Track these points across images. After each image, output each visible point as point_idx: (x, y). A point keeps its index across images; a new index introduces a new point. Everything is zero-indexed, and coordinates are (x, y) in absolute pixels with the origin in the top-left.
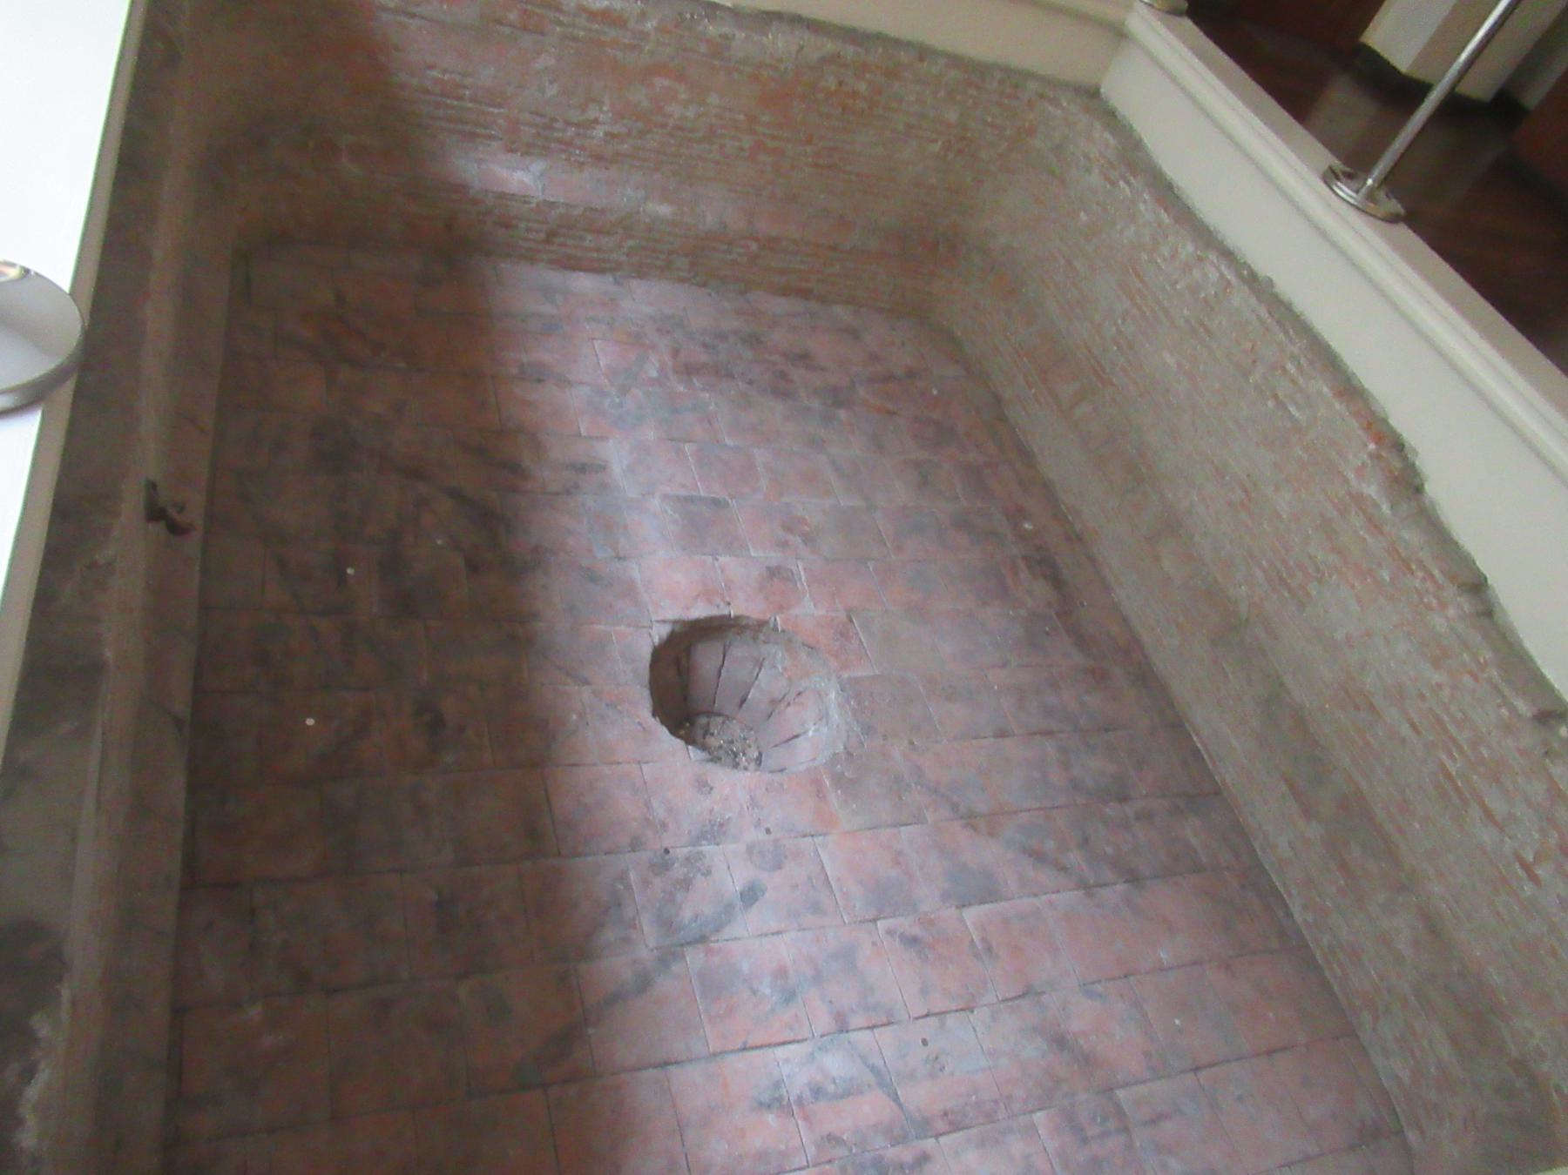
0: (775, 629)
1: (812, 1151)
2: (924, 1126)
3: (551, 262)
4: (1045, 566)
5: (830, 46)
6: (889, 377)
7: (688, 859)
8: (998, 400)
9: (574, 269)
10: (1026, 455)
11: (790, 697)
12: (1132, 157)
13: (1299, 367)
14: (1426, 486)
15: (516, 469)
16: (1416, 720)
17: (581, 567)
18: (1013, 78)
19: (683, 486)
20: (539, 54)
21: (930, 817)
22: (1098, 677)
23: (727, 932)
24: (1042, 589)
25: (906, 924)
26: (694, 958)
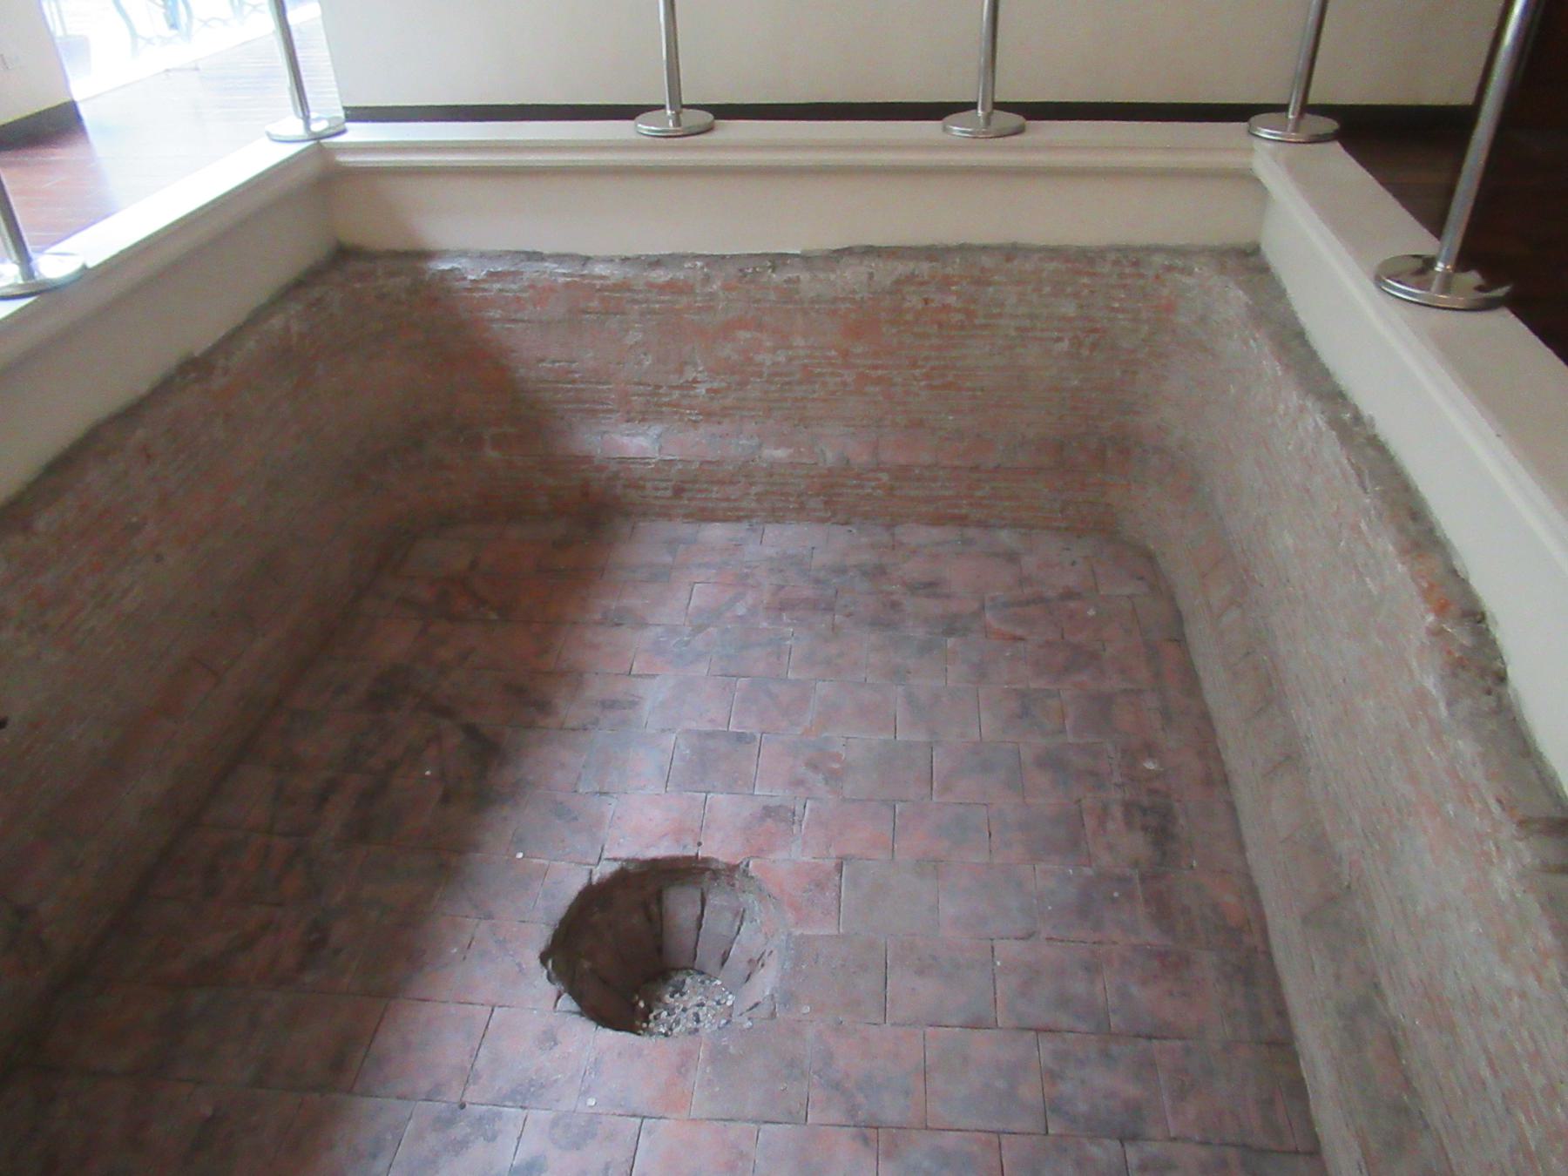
0: (745, 873)
3: (686, 516)
4: (1158, 822)
5: (902, 268)
6: (1040, 600)
7: (481, 1118)
15: (544, 706)
18: (1132, 258)
19: (712, 721)
20: (627, 331)
22: (1170, 963)
24: (1135, 844)
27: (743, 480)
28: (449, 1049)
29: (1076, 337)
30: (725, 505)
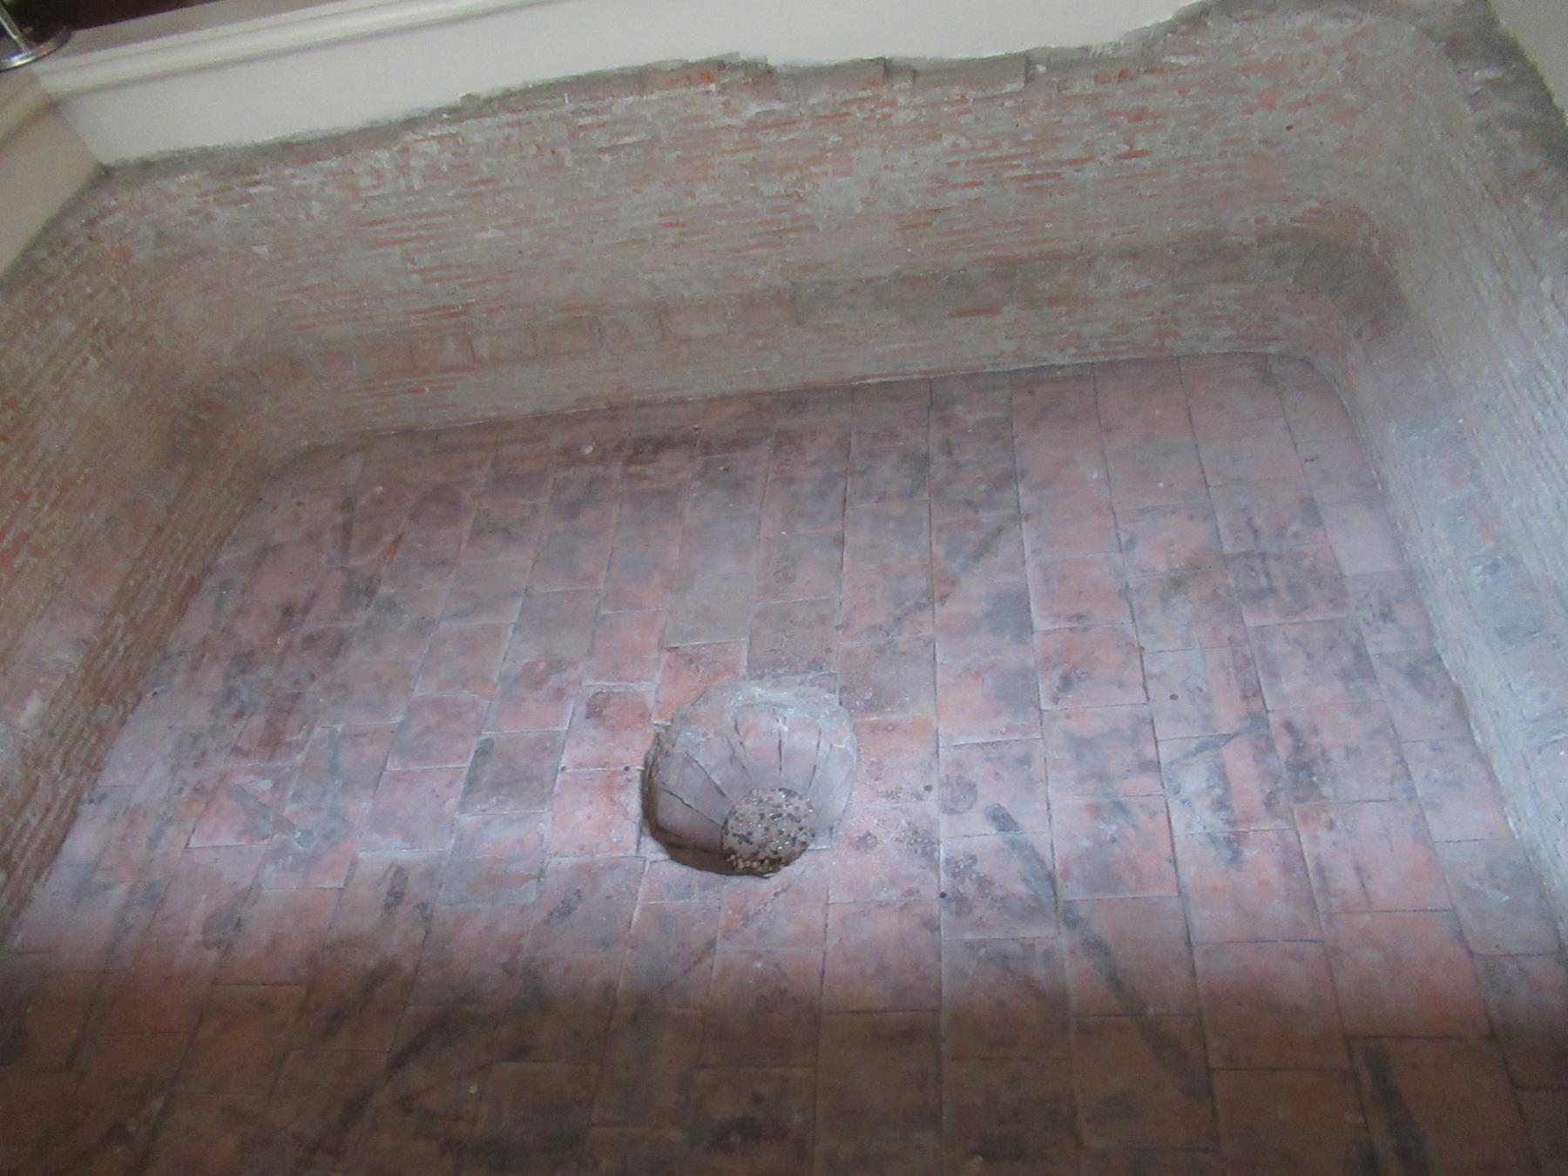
0: (667, 728)
1: (1280, 824)
2: (1257, 719)
3: (37, 877)
7: (955, 875)
8: (409, 432)
9: (57, 850)
10: (495, 426)
11: (735, 739)
12: (234, 168)
13: (589, 112)
14: (771, 62)
15: (375, 979)
16: (969, 179)
17: (547, 922)
19: (450, 784)
21: (928, 632)
22: (786, 440)
23: (1044, 851)
25: (1046, 686)
26: (1072, 891)
27: (39, 772)
28: (881, 928)
29: (93, 346)
30: (51, 817)
